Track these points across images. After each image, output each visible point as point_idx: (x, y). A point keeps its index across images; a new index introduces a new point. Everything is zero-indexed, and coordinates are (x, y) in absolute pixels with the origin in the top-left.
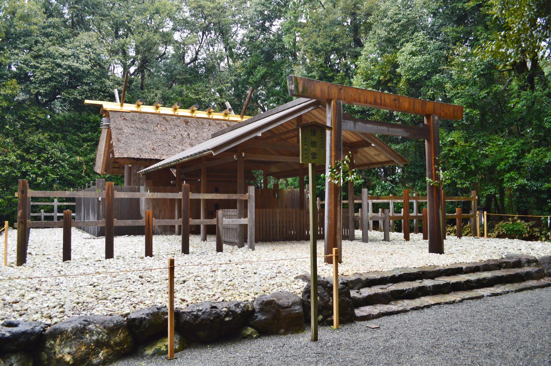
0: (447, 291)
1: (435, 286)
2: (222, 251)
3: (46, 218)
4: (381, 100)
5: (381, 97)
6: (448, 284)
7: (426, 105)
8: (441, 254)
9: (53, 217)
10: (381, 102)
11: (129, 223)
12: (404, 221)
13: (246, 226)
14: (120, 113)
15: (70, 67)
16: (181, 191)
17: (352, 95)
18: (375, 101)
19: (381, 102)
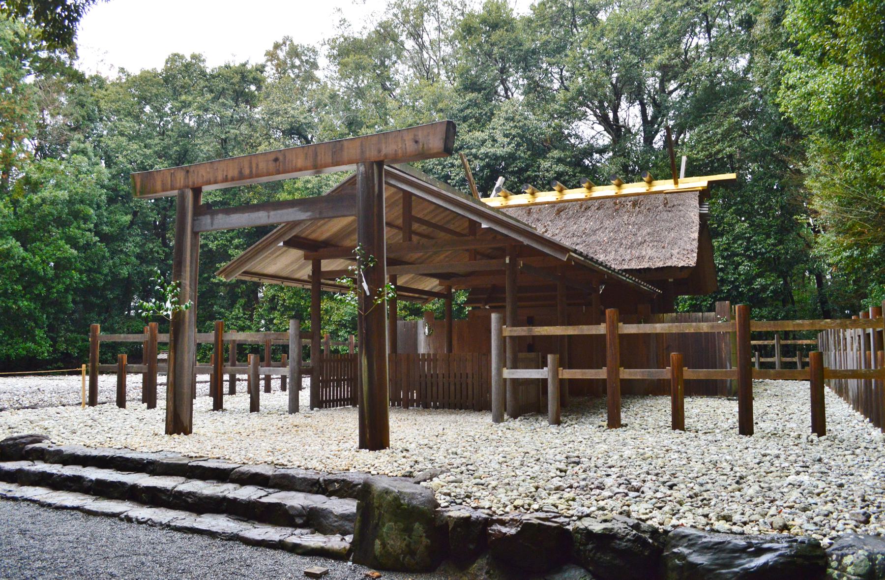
0: (116, 495)
1: (100, 483)
2: (258, 410)
3: (785, 365)
4: (251, 167)
5: (251, 163)
6: (122, 484)
7: (342, 149)
8: (186, 434)
9: (774, 363)
10: (251, 171)
11: (702, 374)
12: (876, 382)
13: (545, 381)
14: (661, 197)
15: (486, 155)
16: (604, 322)
17: (204, 174)
18: (241, 172)
19: (251, 171)
